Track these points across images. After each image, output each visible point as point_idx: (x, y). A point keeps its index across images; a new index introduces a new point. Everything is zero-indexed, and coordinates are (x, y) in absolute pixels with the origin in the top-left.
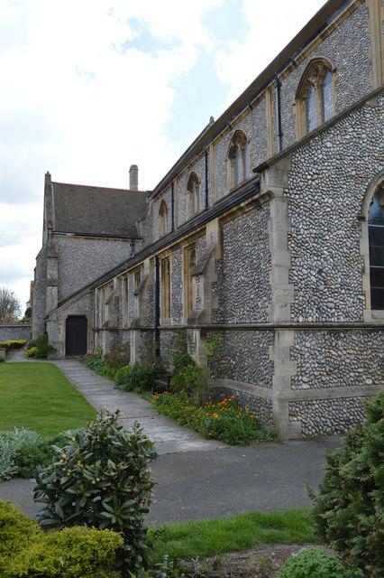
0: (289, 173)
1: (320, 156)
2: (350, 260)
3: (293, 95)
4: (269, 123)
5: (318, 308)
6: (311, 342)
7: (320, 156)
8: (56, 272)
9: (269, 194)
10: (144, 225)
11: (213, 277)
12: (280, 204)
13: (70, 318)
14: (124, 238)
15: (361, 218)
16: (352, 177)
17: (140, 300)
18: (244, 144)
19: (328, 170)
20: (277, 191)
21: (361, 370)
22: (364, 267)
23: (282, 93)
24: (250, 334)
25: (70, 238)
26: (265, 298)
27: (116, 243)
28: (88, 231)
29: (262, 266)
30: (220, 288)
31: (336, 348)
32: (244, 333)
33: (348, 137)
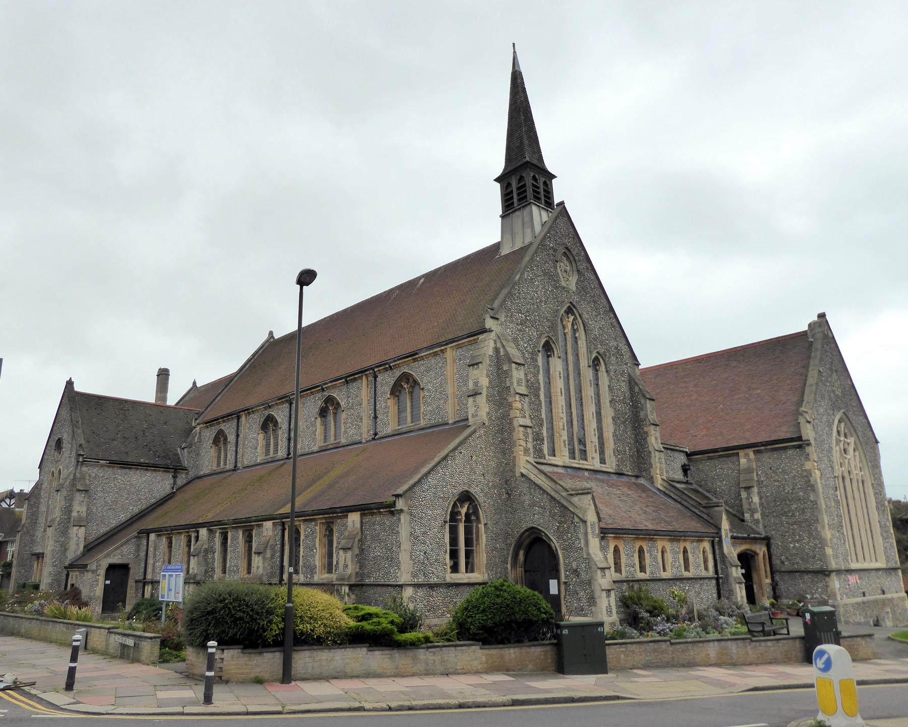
0: (411, 498)
1: (426, 487)
2: (441, 545)
3: (388, 390)
4: (365, 403)
5: (424, 574)
6: (421, 593)
7: (426, 487)
8: (84, 509)
9: (401, 511)
10: (189, 453)
11: (357, 551)
12: (406, 515)
13: (112, 568)
14: (166, 469)
15: (445, 522)
16: (441, 498)
17: (264, 558)
18: (336, 409)
19: (429, 495)
20: (405, 509)
21: (445, 609)
22: (446, 549)
23: (378, 383)
24: (384, 589)
25: (103, 466)
26: (396, 568)
27: (155, 474)
28: (124, 458)
29: (394, 549)
30: (361, 558)
31: (432, 596)
32: (379, 588)
33: (439, 475)
